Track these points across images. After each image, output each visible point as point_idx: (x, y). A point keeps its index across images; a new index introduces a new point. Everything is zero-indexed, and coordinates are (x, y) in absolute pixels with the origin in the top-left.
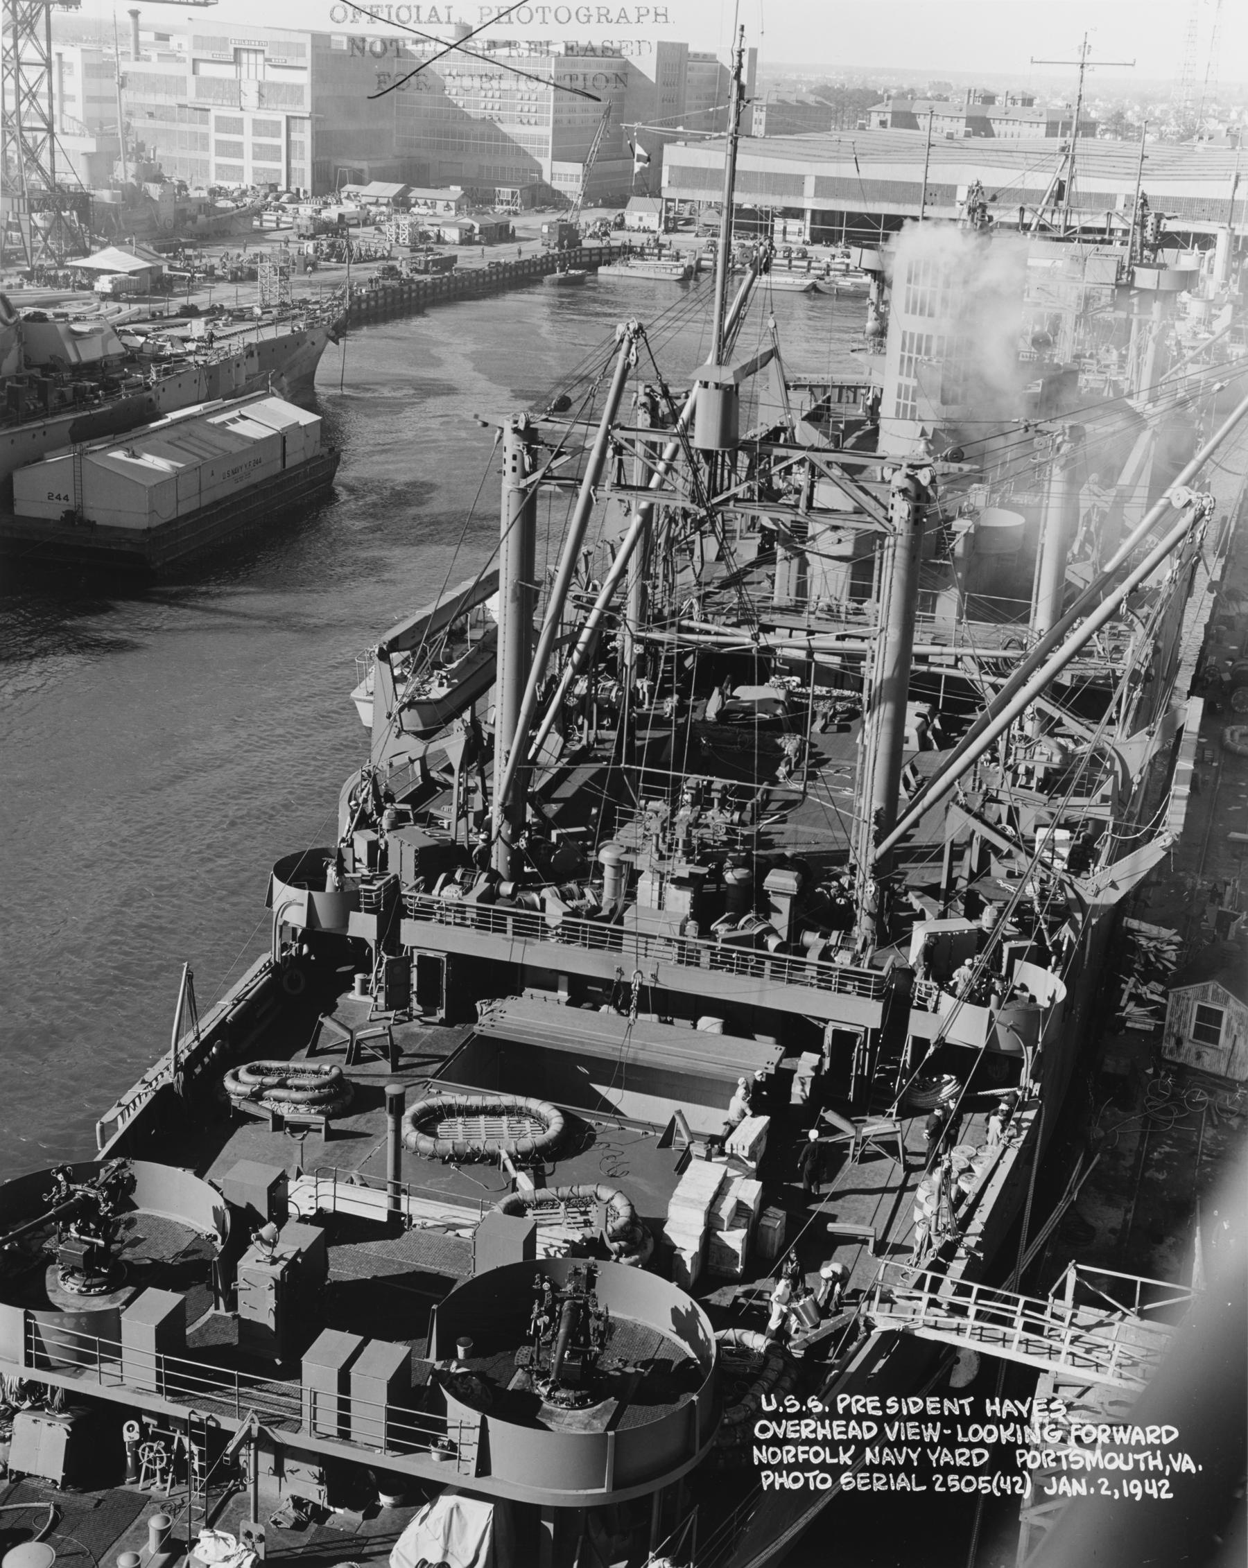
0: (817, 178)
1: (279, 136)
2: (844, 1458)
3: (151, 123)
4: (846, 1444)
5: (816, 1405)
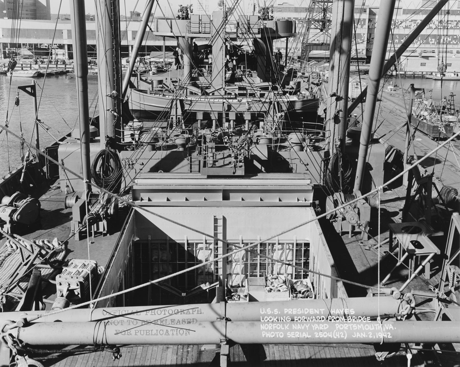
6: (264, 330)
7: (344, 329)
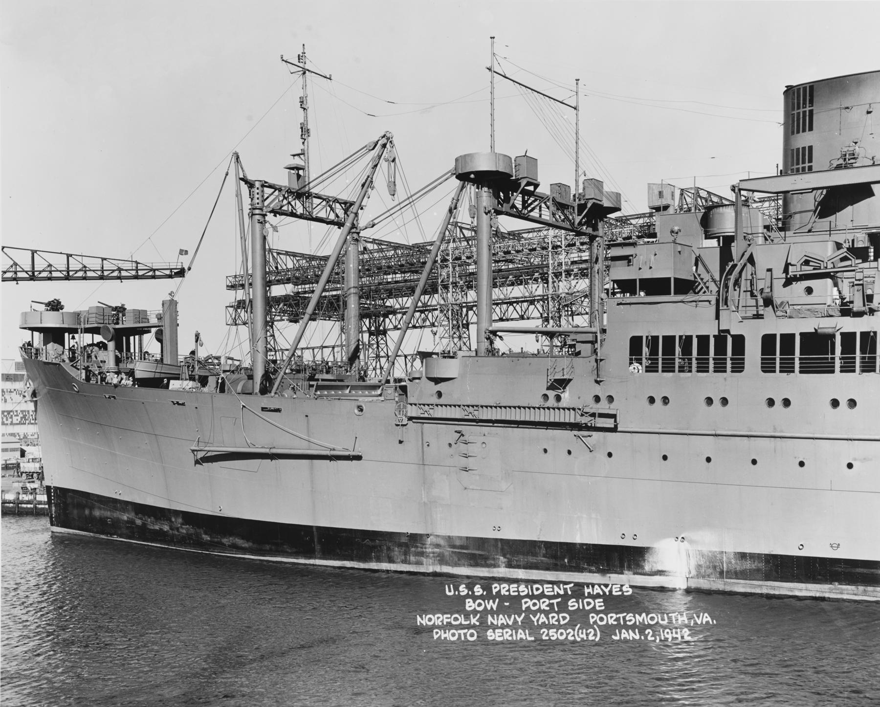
7: (657, 623)
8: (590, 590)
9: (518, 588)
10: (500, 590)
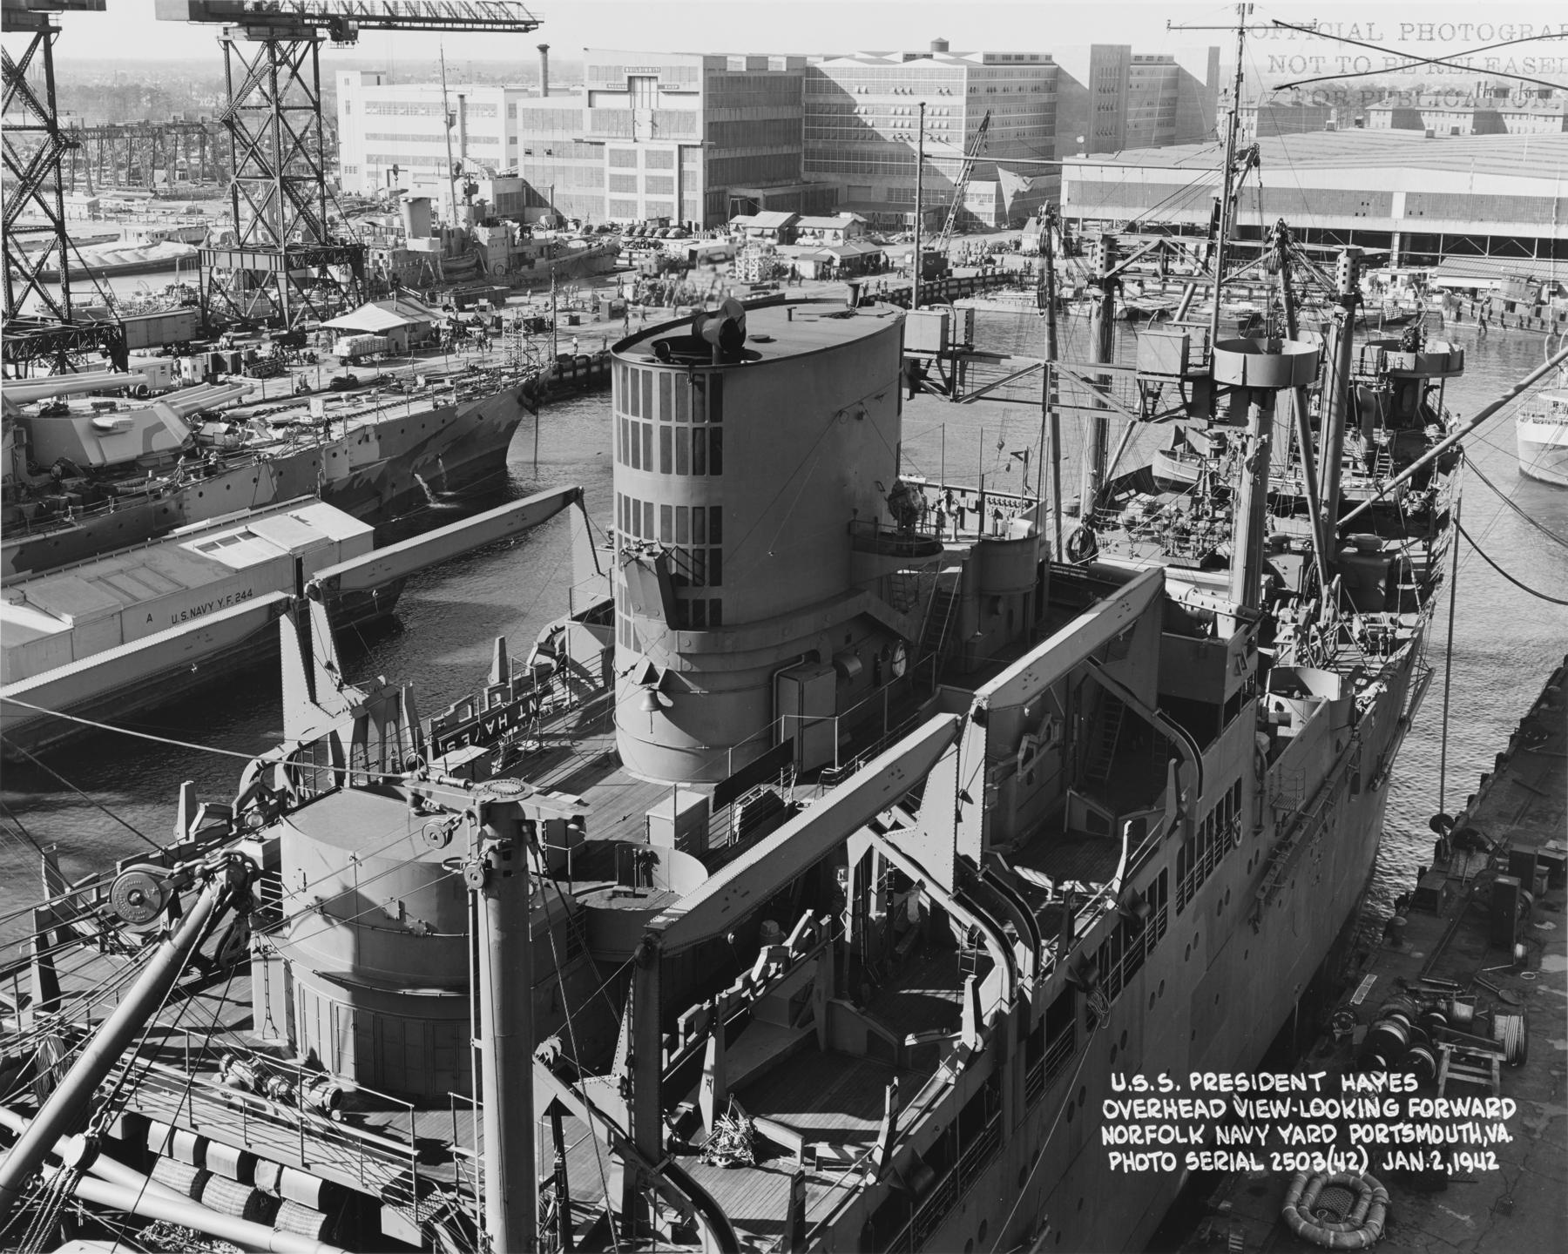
0: (1409, 195)
1: (671, 167)
2: (1196, 1137)
3: (549, 161)
4: (1195, 1123)
5: (1166, 1083)
6: (1116, 1147)
8: (1351, 1083)
9: (1402, 1079)
10: (1202, 1084)
